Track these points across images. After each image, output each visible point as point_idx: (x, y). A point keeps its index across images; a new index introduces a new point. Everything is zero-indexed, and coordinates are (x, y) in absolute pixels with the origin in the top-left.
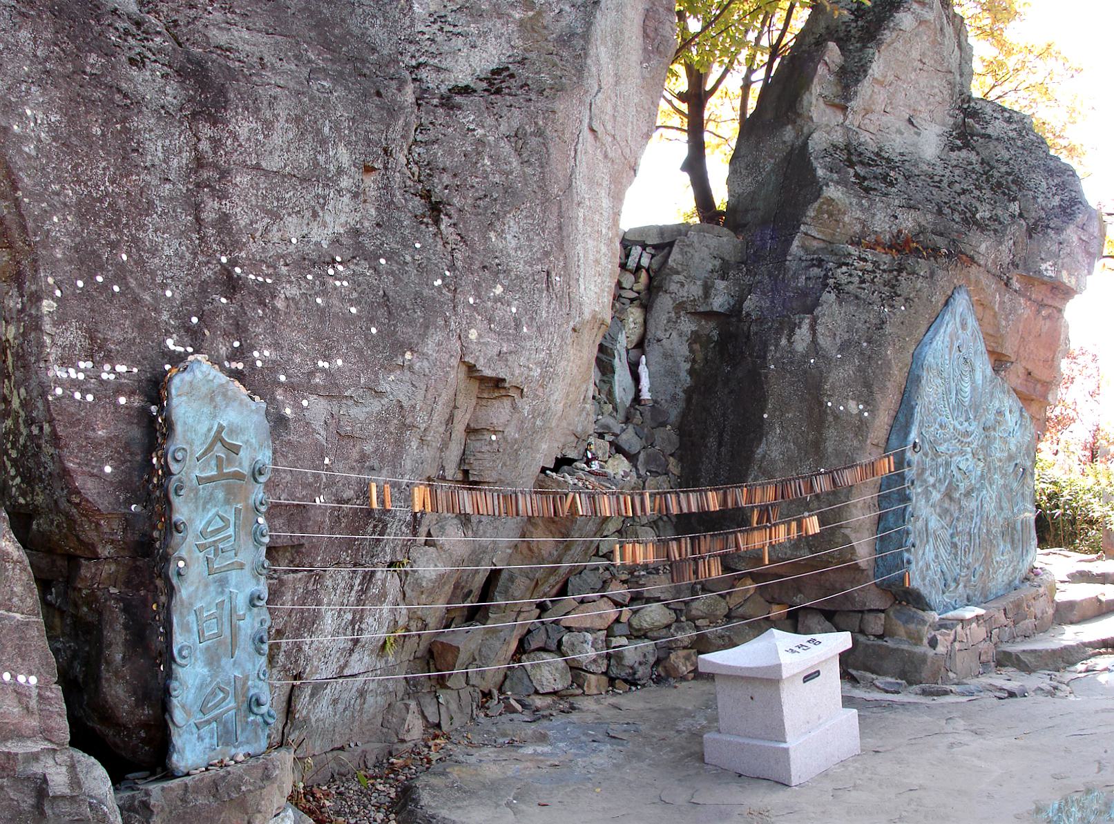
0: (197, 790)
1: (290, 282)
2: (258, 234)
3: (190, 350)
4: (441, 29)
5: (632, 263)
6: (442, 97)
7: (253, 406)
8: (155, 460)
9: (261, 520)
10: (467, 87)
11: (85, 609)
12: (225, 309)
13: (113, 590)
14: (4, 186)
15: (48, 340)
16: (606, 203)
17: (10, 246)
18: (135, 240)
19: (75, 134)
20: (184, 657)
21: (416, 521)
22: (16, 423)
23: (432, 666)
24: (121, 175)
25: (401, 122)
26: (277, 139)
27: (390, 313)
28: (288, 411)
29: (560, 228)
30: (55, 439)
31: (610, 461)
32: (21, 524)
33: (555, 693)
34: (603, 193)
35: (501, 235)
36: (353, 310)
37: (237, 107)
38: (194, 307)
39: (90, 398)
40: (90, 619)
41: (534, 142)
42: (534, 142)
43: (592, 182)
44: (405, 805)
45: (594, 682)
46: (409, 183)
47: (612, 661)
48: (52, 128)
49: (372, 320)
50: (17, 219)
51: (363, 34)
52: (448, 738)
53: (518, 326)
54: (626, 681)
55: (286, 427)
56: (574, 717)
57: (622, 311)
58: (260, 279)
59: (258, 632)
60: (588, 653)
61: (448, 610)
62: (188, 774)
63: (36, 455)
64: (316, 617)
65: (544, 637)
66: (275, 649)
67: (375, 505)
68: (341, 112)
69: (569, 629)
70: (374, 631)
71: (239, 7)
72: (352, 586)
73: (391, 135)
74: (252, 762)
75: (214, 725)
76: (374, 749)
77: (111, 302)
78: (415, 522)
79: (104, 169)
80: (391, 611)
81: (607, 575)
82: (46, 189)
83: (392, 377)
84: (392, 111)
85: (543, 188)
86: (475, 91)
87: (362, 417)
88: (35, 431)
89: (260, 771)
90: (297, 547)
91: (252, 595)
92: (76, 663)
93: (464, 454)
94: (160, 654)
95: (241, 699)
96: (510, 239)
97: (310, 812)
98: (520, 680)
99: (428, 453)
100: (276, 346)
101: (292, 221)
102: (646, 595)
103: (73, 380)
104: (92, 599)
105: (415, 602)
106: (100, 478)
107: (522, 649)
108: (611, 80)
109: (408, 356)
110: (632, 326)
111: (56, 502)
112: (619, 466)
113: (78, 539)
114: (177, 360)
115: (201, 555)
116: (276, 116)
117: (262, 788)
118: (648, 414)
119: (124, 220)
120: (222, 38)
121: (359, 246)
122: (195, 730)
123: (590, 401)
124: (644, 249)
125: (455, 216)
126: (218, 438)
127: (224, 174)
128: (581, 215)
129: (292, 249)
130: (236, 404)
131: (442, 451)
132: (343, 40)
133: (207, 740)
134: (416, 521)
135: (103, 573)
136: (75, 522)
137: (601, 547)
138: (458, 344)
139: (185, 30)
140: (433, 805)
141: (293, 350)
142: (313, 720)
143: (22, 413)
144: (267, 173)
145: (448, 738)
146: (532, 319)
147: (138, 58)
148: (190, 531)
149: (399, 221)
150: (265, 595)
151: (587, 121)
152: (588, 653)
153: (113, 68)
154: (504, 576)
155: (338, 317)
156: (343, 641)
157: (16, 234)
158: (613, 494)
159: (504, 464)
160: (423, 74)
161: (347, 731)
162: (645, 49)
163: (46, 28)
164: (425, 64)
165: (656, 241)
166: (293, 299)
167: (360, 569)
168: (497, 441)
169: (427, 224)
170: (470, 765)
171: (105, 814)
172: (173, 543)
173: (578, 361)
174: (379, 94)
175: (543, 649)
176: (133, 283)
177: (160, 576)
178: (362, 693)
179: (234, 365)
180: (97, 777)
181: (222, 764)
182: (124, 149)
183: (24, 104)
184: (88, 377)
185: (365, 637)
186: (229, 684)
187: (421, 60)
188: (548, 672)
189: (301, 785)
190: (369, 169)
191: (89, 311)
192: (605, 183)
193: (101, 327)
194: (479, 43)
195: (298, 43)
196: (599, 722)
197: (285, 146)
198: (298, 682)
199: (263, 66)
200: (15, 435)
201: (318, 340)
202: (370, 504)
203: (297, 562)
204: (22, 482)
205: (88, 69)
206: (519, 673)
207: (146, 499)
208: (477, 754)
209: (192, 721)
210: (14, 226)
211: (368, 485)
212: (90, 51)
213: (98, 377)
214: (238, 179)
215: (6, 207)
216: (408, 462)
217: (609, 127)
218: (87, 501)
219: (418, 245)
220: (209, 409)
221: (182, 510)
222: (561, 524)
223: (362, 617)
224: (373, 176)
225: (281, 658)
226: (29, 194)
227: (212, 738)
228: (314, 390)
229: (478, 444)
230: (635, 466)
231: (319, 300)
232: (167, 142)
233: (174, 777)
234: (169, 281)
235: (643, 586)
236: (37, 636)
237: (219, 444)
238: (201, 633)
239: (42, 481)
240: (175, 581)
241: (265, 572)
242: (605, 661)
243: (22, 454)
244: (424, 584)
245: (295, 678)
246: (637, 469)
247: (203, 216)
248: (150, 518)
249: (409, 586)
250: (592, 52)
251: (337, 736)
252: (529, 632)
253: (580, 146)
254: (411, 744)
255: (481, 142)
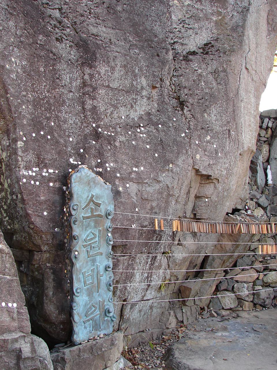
0: (84, 351)
1: (122, 135)
2: (108, 115)
3: (80, 163)
4: (183, 26)
5: (264, 126)
6: (184, 56)
7: (106, 186)
8: (65, 210)
9: (109, 235)
10: (194, 52)
11: (37, 273)
12: (95, 146)
13: (48, 265)
14: (2, 92)
15: (20, 159)
16: (253, 100)
17: (4, 118)
18: (57, 117)
19: (33, 70)
20: (78, 293)
21: (174, 235)
22: (6, 194)
23: (180, 296)
24: (52, 89)
25: (167, 67)
26: (116, 75)
27: (163, 148)
28: (121, 189)
29: (234, 111)
30: (23, 201)
31: (256, 210)
32: (9, 237)
33: (231, 309)
34: (252, 96)
35: (209, 115)
36: (148, 147)
37: (100, 61)
38: (81, 145)
39: (38, 183)
40: (38, 277)
41: (222, 74)
42: (222, 74)
43: (247, 91)
44: (168, 357)
45: (247, 305)
46: (171, 93)
47: (255, 296)
48: (23, 67)
49: (156, 151)
50: (7, 106)
51: (151, 29)
52: (186, 328)
53: (217, 153)
54: (261, 305)
55: (120, 195)
56: (239, 320)
57: (261, 146)
58: (109, 134)
59: (109, 282)
60: (245, 292)
61: (187, 272)
62: (80, 344)
63: (15, 208)
64: (133, 275)
65: (227, 285)
66: (115, 288)
67: (157, 228)
68: (143, 63)
69: (237, 281)
70: (156, 281)
71: (101, 17)
72: (147, 262)
73: (163, 73)
74: (106, 337)
75: (91, 321)
76: (156, 332)
77: (47, 143)
78: (174, 235)
79: (45, 86)
80: (163, 272)
81: (254, 259)
82: (20, 94)
83: (164, 175)
84: (164, 63)
85: (226, 94)
86: (197, 53)
87: (152, 191)
88: (15, 197)
89: (110, 341)
90: (125, 246)
91: (106, 266)
92: (33, 297)
93: (194, 207)
94: (68, 292)
95: (102, 310)
96: (213, 116)
97: (130, 360)
98: (216, 303)
99: (179, 206)
100: (116, 161)
101: (122, 109)
102: (270, 268)
103: (30, 176)
104: (39, 269)
105: (173, 269)
106: (42, 217)
107: (217, 290)
108: (254, 46)
109: (171, 166)
110: (265, 152)
111: (23, 227)
112: (259, 212)
113: (33, 243)
114: (75, 167)
115: (85, 249)
116: (116, 65)
117: (111, 349)
118: (271, 190)
119: (53, 108)
120: (94, 30)
121: (150, 120)
122: (83, 324)
123: (247, 184)
124: (270, 119)
125: (190, 107)
126: (91, 200)
127: (95, 89)
128: (242, 105)
129: (122, 121)
130: (99, 186)
131: (185, 205)
132: (143, 32)
133: (88, 328)
134: (174, 235)
135: (44, 258)
136: (32, 236)
137: (251, 247)
138: (192, 161)
139: (79, 26)
140: (180, 357)
141: (123, 163)
142: (131, 319)
143: (9, 190)
144: (112, 89)
145: (186, 328)
146: (222, 150)
147: (60, 38)
148: (80, 239)
149: (167, 109)
150: (111, 266)
151: (244, 65)
152: (245, 292)
153: (49, 42)
154: (210, 258)
155: (142, 149)
156: (144, 285)
157: (7, 113)
158: (257, 224)
159: (211, 211)
160: (176, 46)
161: (145, 324)
162: (268, 30)
163: (21, 21)
164: (177, 42)
165: (275, 116)
166: (123, 142)
167: (151, 255)
168: (208, 202)
169: (178, 110)
170: (195, 340)
171: (46, 365)
172: (73, 244)
173: (242, 168)
174: (158, 55)
175: (226, 290)
176: (56, 135)
177: (67, 258)
178: (151, 308)
179: (98, 170)
180: (42, 347)
181: (94, 339)
182: (53, 78)
183: (11, 56)
184: (37, 175)
185: (153, 283)
186: (97, 304)
187: (175, 40)
188: (228, 300)
189: (127, 348)
190: (154, 87)
191: (37, 146)
192: (252, 92)
193: (42, 153)
194: (199, 32)
195: (125, 33)
196: (249, 323)
197: (120, 78)
198: (125, 303)
199: (111, 43)
200: (6, 199)
201: (133, 159)
202: (155, 228)
203: (124, 252)
204: (9, 219)
205: (39, 42)
206: (216, 300)
207: (61, 226)
208: (198, 335)
209: (82, 320)
210: (6, 110)
211: (154, 220)
212: (40, 34)
213: (41, 175)
214: (100, 91)
215: (3, 101)
216: (171, 210)
217: (254, 67)
218: (37, 227)
219: (175, 119)
220: (88, 188)
221: (77, 231)
222: (234, 237)
223: (151, 275)
224: (156, 90)
225: (118, 292)
226: (13, 96)
227: (90, 327)
228: (132, 180)
229: (200, 203)
230: (266, 212)
231: (133, 143)
232: (71, 75)
233: (75, 345)
234: (71, 134)
235: (269, 264)
236: (16, 286)
237: (92, 203)
238: (85, 283)
239: (17, 218)
240: (74, 260)
241: (111, 256)
242: (252, 296)
243: (9, 207)
244: (177, 261)
245: (124, 301)
246: (266, 214)
247: (86, 107)
248: (63, 234)
249: (171, 262)
250: (246, 34)
251: (141, 326)
252: (220, 282)
253: (241, 76)
254: (171, 330)
255: (200, 75)
